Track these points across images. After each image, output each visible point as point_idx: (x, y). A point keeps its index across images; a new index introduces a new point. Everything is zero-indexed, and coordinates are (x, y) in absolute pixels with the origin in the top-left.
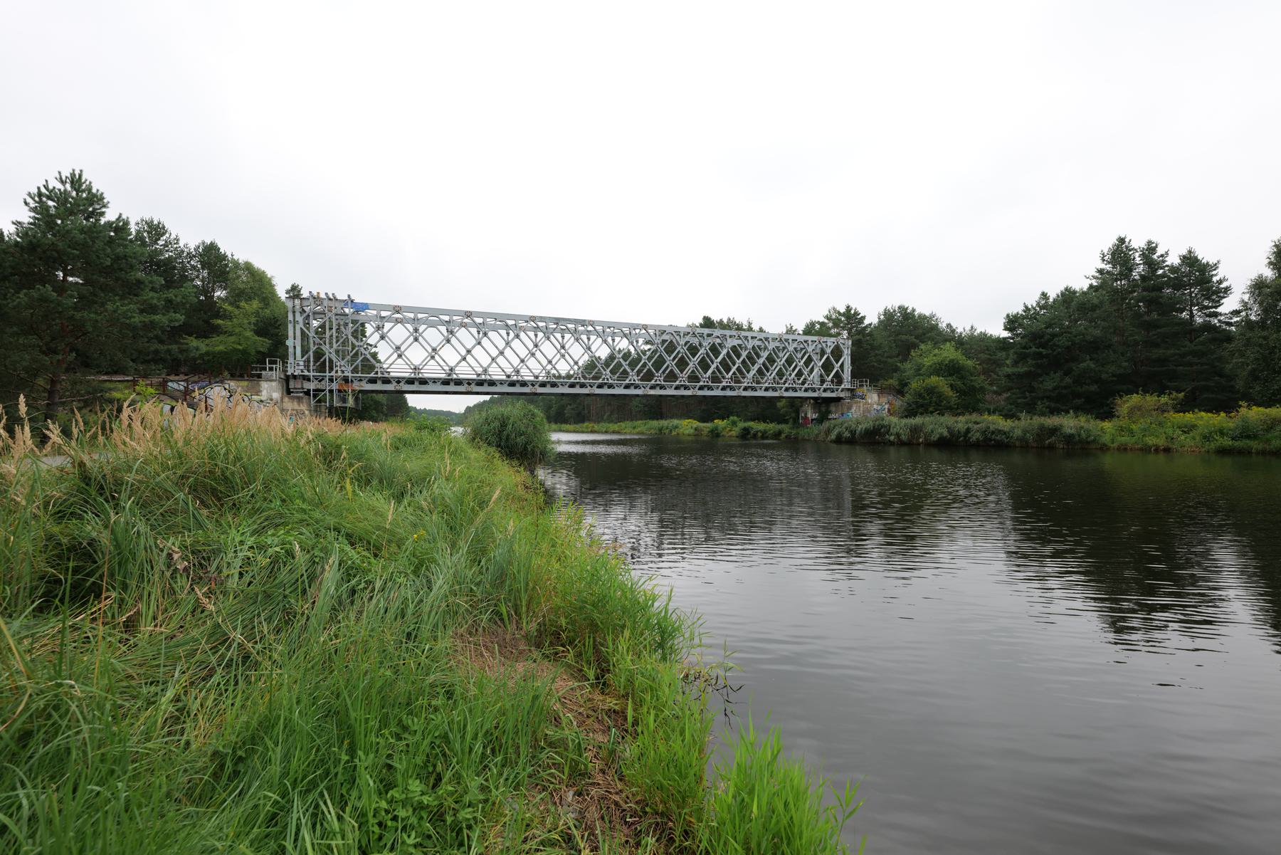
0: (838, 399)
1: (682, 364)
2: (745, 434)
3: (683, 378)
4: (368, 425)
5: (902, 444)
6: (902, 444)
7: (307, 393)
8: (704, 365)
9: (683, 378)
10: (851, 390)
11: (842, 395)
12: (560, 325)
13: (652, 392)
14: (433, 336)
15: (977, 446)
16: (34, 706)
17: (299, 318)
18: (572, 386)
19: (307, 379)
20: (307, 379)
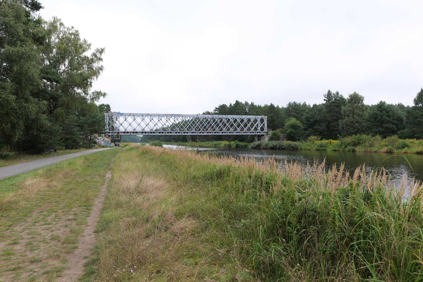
0: (263, 135)
1: (239, 126)
2: (237, 146)
3: (246, 129)
4: (354, 177)
5: (264, 149)
6: (264, 149)
7: (109, 136)
8: (245, 125)
9: (239, 129)
10: (267, 132)
11: (264, 134)
12: (179, 115)
13: (200, 134)
14: (147, 119)
15: (279, 149)
16: (22, 228)
17: (107, 118)
18: (160, 133)
19: (110, 133)
20: (110, 133)
